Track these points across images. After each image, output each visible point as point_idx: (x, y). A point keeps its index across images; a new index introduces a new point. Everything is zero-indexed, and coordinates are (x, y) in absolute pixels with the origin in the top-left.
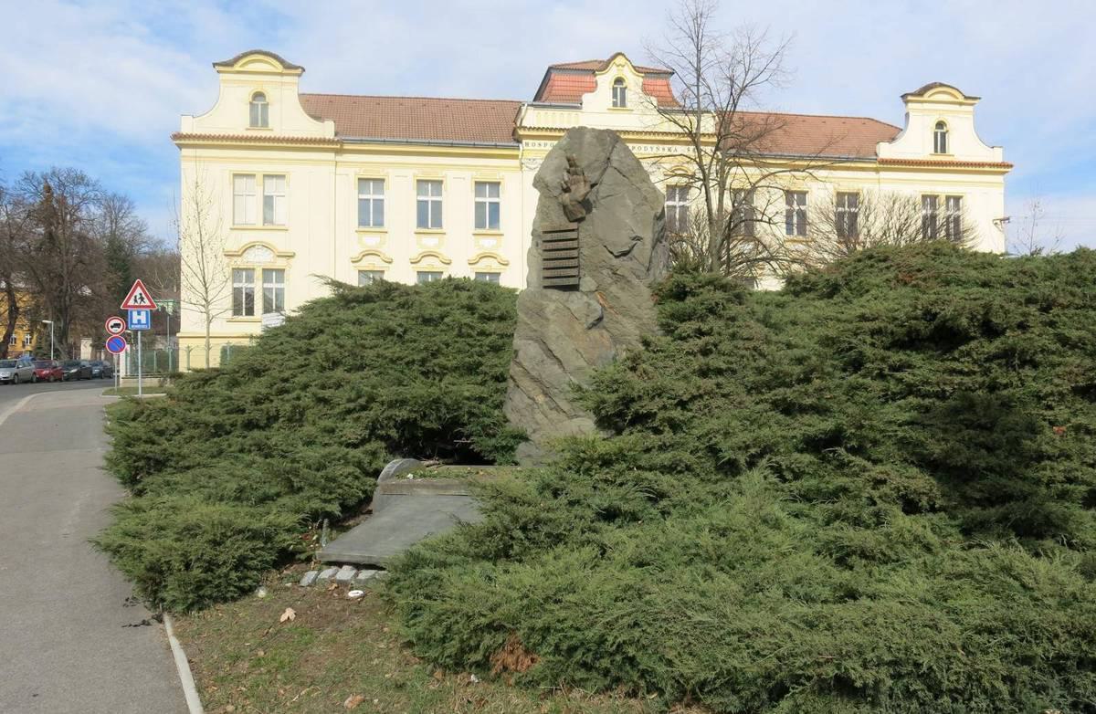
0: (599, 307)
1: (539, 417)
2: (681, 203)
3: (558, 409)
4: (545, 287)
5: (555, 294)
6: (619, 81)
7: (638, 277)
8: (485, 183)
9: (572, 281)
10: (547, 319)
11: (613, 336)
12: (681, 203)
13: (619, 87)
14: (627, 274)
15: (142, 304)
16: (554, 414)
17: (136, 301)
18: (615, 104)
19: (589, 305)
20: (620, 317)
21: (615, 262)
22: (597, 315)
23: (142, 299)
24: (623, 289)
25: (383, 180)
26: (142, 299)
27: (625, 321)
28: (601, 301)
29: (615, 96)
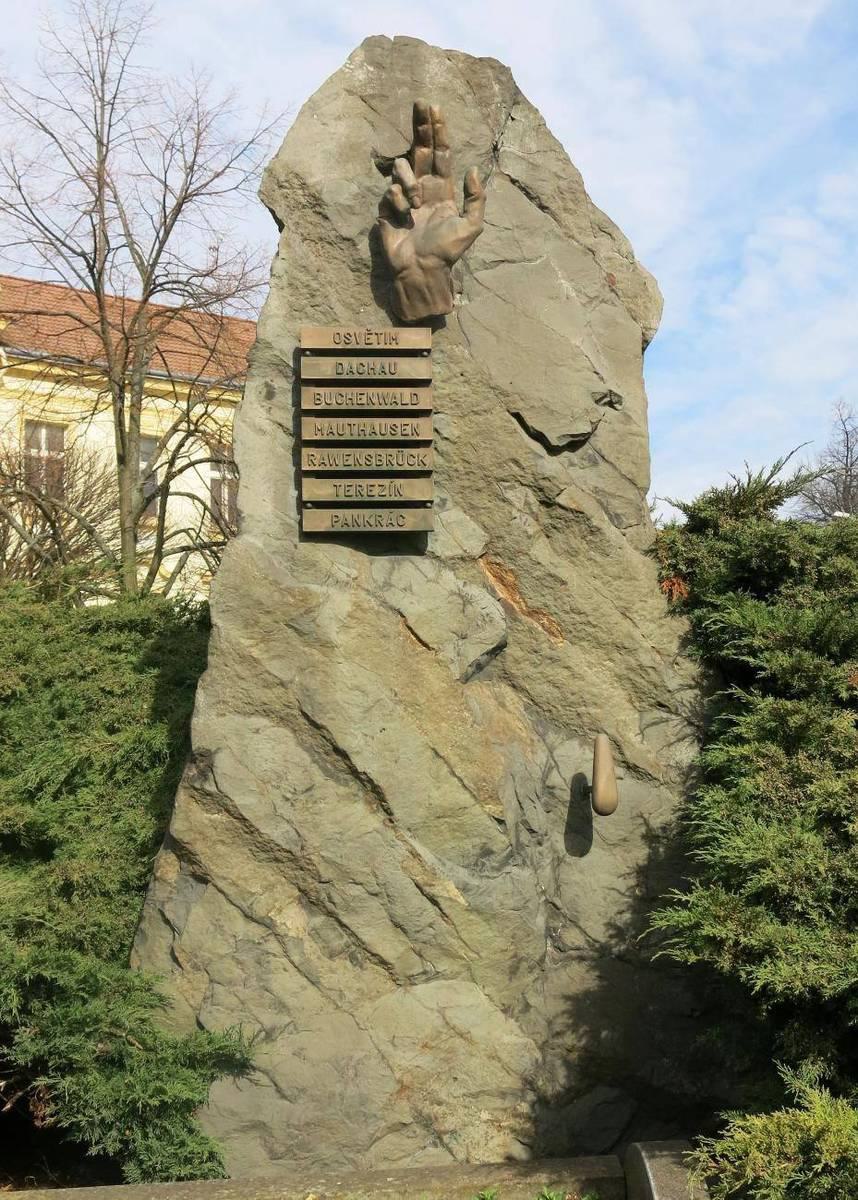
0: (497, 611)
1: (286, 982)
3: (360, 953)
4: (309, 537)
5: (343, 560)
7: (615, 519)
9: (410, 521)
10: (326, 645)
11: (533, 704)
14: (590, 507)
16: (341, 974)
19: (466, 601)
20: (561, 644)
21: (551, 465)
22: (490, 636)
24: (572, 554)
27: (577, 656)
28: (502, 593)
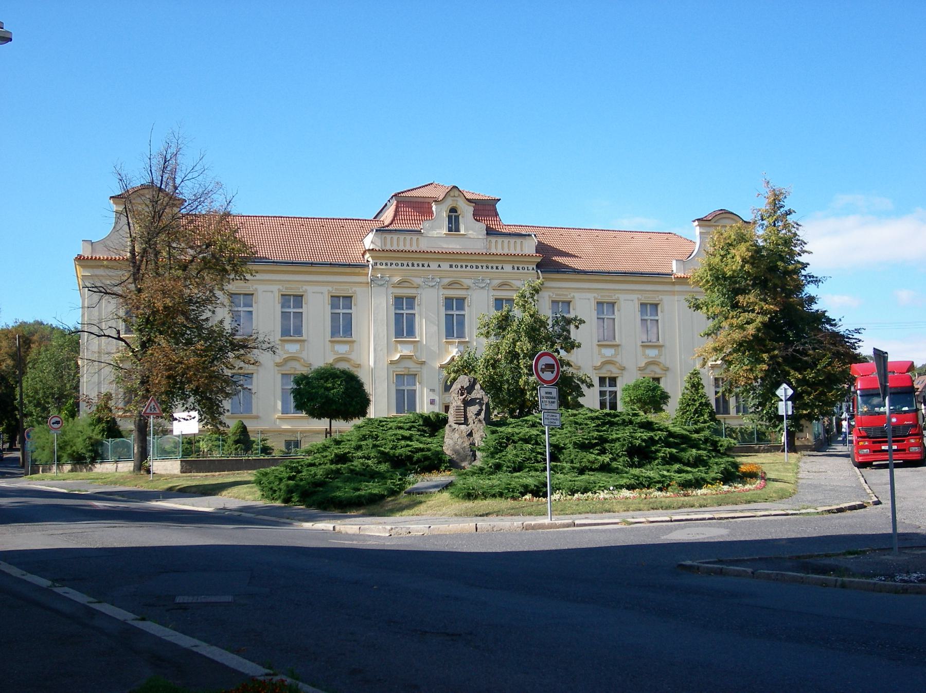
2: (458, 313)
6: (453, 210)
8: (338, 297)
12: (458, 313)
13: (453, 214)
15: (155, 412)
17: (151, 410)
18: (450, 230)
23: (155, 408)
25: (252, 294)
26: (155, 408)
29: (450, 222)
